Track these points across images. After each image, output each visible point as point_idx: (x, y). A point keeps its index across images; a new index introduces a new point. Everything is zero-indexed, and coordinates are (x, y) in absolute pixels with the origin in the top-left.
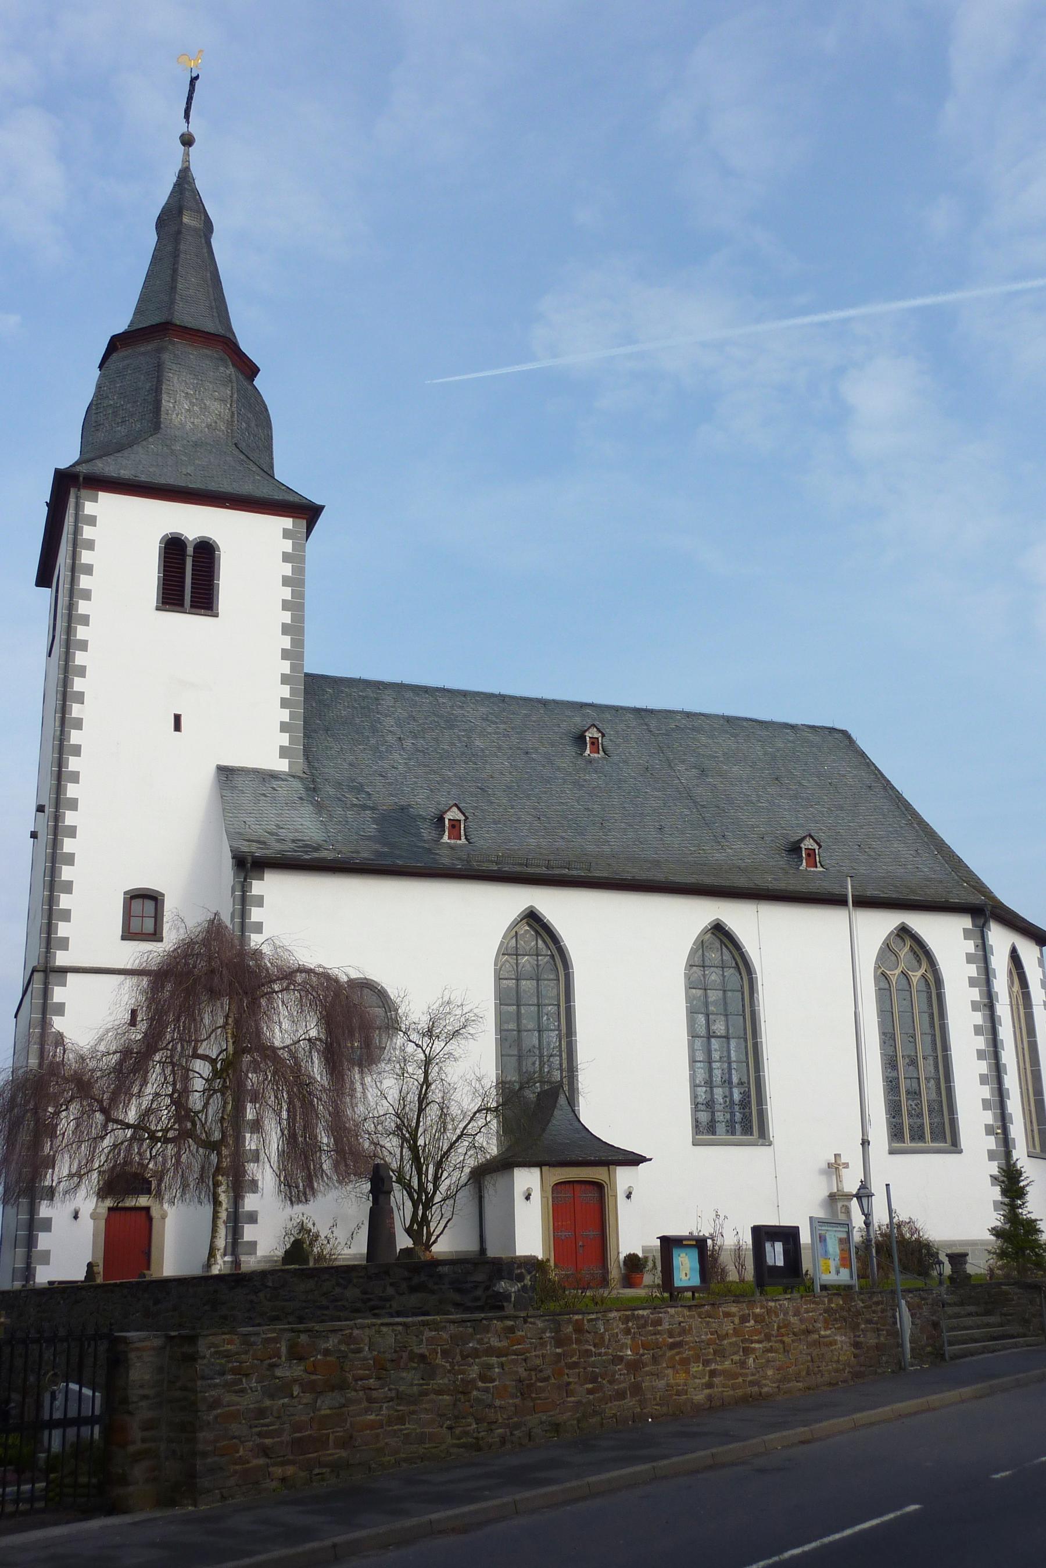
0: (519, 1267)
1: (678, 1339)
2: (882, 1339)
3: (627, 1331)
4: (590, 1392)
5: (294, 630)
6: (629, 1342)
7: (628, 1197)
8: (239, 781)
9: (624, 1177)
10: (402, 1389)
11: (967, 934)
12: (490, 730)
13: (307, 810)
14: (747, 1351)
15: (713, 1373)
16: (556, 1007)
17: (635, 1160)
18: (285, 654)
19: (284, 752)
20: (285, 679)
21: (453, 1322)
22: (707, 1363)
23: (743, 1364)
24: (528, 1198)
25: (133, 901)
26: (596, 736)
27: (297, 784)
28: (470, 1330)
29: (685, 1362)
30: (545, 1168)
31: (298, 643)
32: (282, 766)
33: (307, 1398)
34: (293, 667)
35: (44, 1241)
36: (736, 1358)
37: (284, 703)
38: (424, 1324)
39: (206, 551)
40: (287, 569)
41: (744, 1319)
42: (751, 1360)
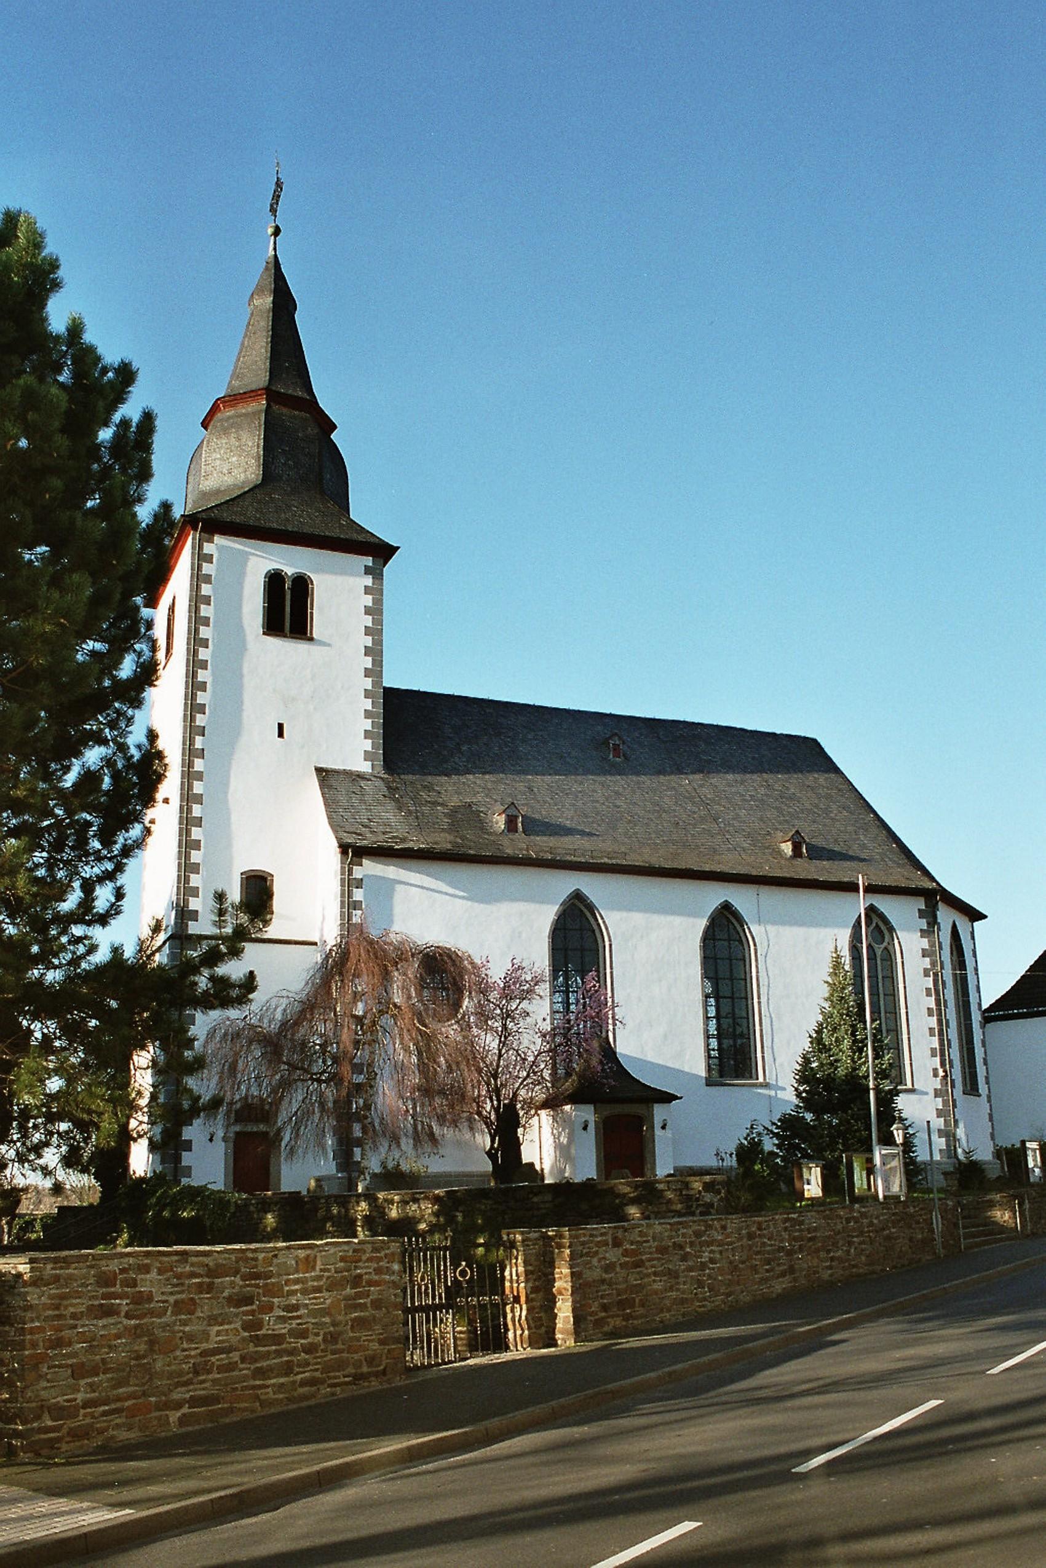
0: (718, 1184)
1: (813, 1234)
2: (925, 1234)
3: (786, 1229)
4: (767, 1271)
5: (375, 652)
6: (787, 1237)
7: (663, 1127)
8: (343, 787)
9: (660, 1112)
10: (670, 1267)
11: (922, 914)
12: (530, 737)
13: (390, 805)
14: (850, 1243)
15: (832, 1259)
16: (721, 994)
17: (668, 1098)
18: (368, 673)
19: (368, 756)
20: (367, 694)
21: (694, 1222)
22: (828, 1251)
23: (848, 1252)
24: (585, 1128)
25: (988, 1025)
26: (617, 742)
27: (379, 783)
28: (703, 1228)
29: (817, 1251)
30: (598, 1105)
31: (378, 663)
32: (365, 767)
33: (624, 1272)
34: (374, 684)
35: (187, 1159)
36: (845, 1248)
37: (368, 714)
38: (680, 1223)
39: (302, 584)
40: (368, 600)
41: (848, 1221)
42: (852, 1250)
